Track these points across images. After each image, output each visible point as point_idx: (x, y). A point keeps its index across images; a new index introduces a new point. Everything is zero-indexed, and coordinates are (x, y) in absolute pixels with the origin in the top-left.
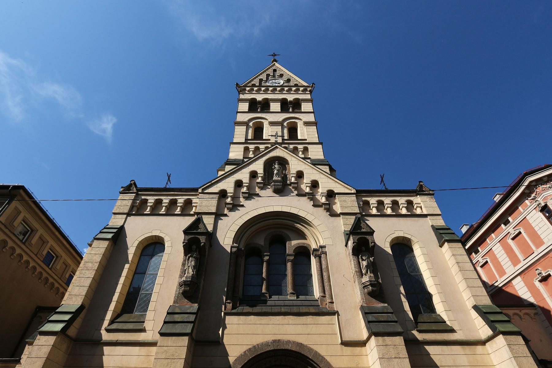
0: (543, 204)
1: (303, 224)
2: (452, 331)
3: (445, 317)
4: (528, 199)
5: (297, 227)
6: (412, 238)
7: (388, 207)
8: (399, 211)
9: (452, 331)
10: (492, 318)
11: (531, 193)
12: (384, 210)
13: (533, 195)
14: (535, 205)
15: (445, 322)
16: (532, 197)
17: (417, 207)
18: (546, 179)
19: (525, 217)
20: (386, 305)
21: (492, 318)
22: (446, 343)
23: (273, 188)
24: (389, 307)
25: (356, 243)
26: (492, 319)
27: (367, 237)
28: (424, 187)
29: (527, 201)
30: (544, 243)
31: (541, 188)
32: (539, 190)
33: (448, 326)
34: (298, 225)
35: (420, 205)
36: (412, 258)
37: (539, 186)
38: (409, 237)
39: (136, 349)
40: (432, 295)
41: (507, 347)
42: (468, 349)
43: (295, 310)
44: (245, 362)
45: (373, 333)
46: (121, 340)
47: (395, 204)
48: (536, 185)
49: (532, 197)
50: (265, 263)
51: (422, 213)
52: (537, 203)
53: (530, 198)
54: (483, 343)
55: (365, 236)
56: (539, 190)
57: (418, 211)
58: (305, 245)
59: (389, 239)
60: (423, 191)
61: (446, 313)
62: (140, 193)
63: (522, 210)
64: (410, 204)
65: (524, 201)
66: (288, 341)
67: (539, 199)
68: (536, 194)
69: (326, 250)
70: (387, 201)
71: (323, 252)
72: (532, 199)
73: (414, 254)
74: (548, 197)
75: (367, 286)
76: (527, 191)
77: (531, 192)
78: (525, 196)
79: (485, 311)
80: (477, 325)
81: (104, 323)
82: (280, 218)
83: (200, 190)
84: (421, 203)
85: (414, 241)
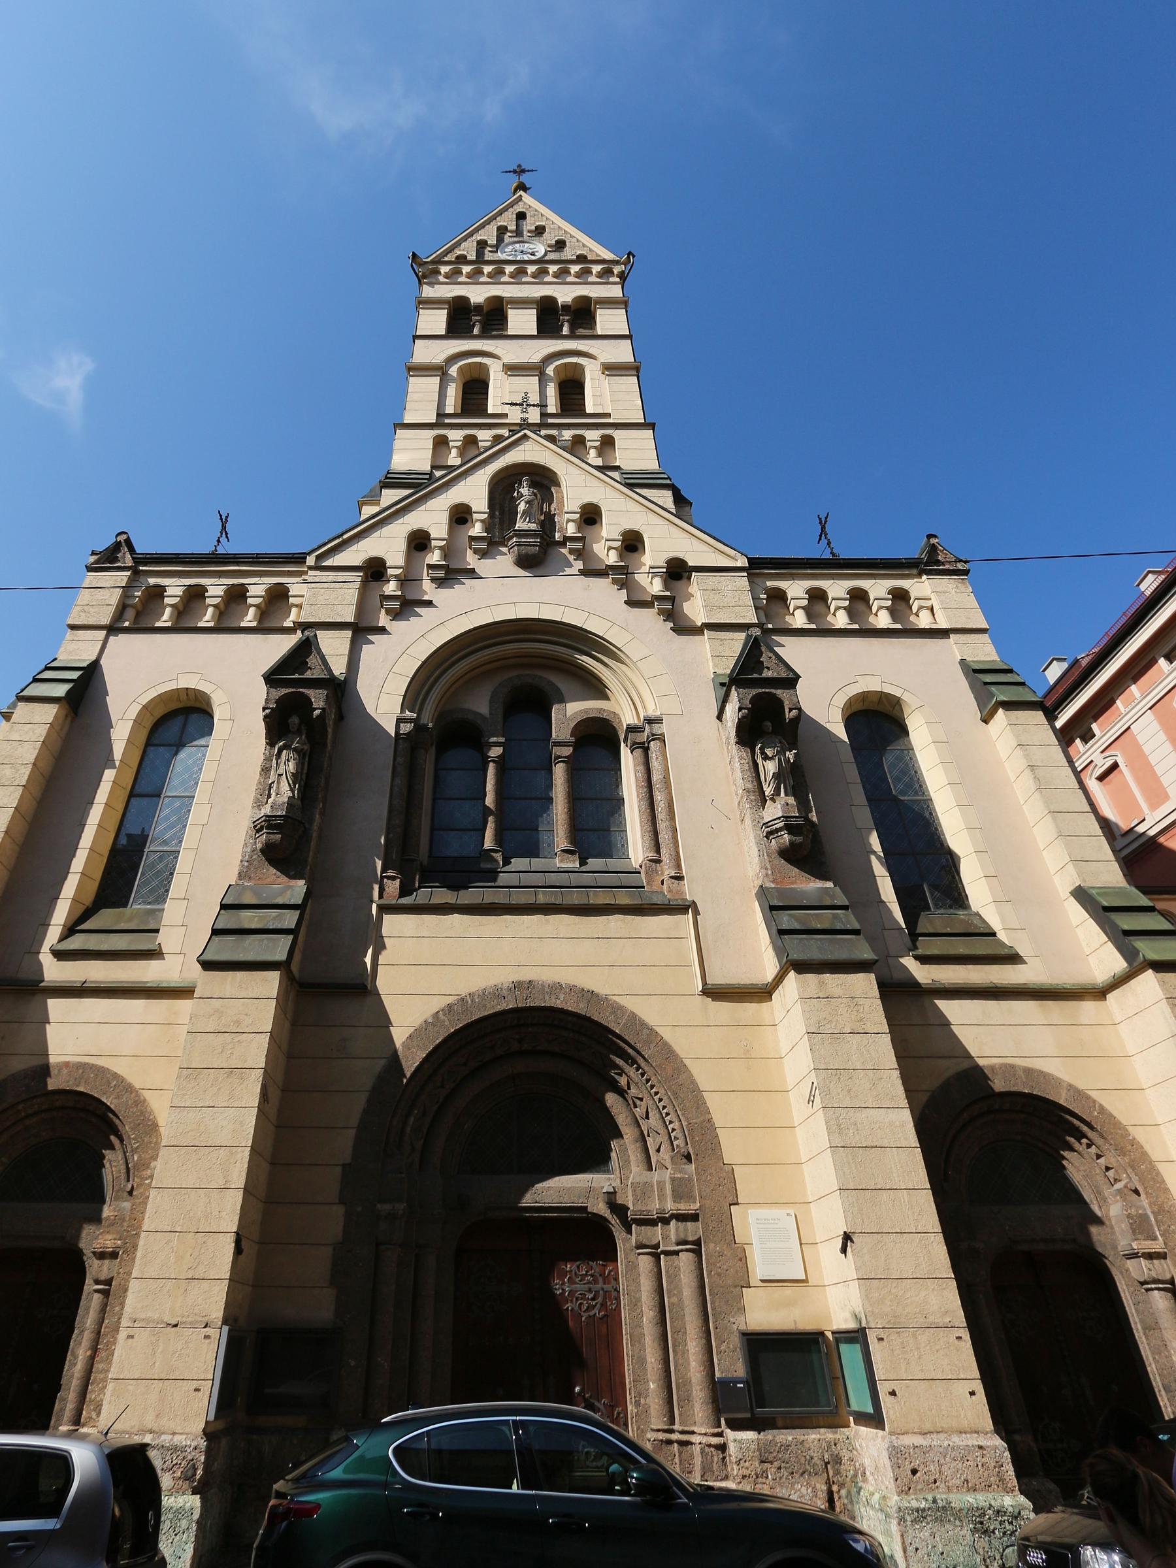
2: (1013, 958)
3: (993, 920)
6: (906, 697)
7: (838, 608)
8: (911, 619)
9: (1013, 958)
15: (994, 934)
20: (830, 885)
23: (516, 552)
25: (745, 709)
33: (1003, 944)
34: (584, 658)
35: (927, 604)
38: (897, 692)
43: (575, 898)
44: (438, 1042)
54: (1100, 993)
55: (773, 691)
57: (924, 621)
59: (841, 700)
69: (664, 728)
71: (653, 735)
73: (910, 742)
75: (777, 830)
79: (1106, 904)
83: (311, 561)
84: (933, 596)
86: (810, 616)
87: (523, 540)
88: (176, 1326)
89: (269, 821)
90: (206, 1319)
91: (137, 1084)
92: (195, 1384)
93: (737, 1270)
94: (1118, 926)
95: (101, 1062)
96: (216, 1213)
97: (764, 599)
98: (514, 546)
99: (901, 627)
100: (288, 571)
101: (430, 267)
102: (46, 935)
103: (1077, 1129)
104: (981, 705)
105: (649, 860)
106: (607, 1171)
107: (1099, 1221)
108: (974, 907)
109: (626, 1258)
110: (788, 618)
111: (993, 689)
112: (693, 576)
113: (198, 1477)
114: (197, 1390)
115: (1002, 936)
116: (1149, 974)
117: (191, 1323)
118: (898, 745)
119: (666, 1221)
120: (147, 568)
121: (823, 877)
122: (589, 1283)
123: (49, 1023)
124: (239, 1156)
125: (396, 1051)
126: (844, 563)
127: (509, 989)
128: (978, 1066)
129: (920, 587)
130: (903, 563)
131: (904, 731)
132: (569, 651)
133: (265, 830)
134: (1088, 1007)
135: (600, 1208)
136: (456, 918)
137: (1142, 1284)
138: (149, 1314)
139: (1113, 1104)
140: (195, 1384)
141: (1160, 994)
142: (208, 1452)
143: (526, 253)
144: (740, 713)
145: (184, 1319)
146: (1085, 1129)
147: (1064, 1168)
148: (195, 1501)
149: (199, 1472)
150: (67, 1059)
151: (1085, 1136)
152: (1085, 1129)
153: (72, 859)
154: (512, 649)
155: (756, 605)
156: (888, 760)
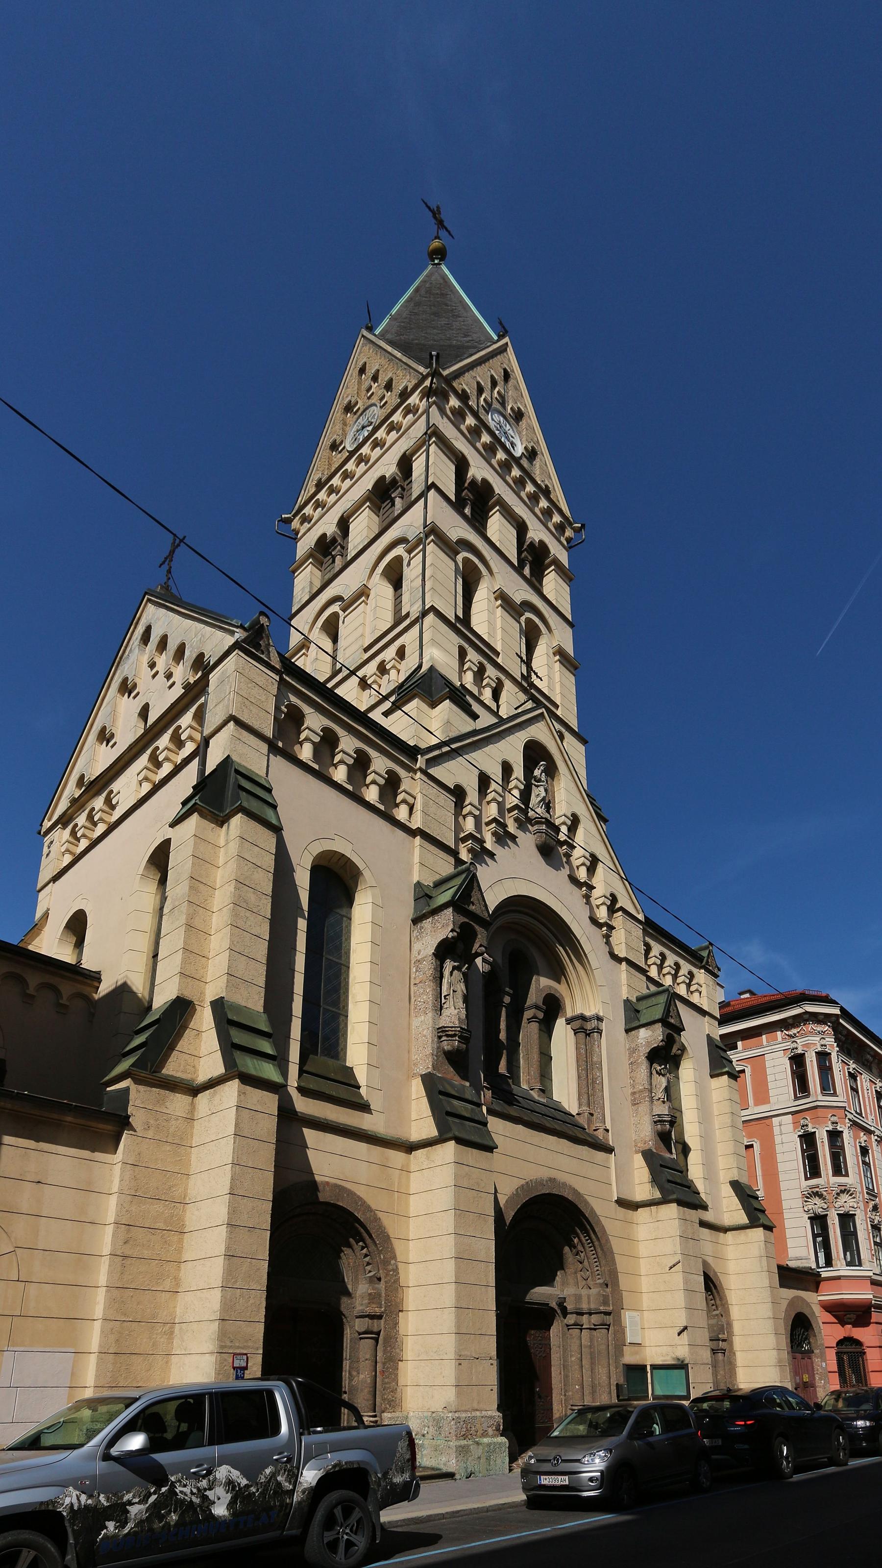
0: (800, 1051)
1: (570, 951)
2: (364, 1107)
3: (361, 1076)
4: (782, 1031)
5: (557, 952)
6: (366, 873)
7: (342, 762)
8: (330, 770)
9: (364, 1107)
10: (239, 1037)
11: (793, 1026)
12: (294, 746)
13: (794, 1031)
14: (789, 1045)
15: (699, 1194)
16: (791, 1033)
17: (404, 801)
18: (821, 1017)
19: (764, 1055)
20: (467, 1084)
21: (239, 1037)
22: (319, 1124)
23: (543, 839)
24: (264, 1017)
25: (484, 946)
26: (236, 1041)
27: (477, 927)
28: (711, 957)
29: (779, 1033)
30: (769, 1102)
31: (811, 1026)
32: (807, 1029)
33: (362, 1098)
34: (561, 948)
35: (410, 800)
36: (345, 919)
37: (809, 1024)
38: (361, 865)
39: (361, 1148)
40: (690, 1150)
41: (762, 1244)
42: (377, 1151)
43: (536, 1118)
44: (519, 1207)
45: (232, 1072)
46: (337, 1123)
47: (361, 764)
48: (807, 1020)
49: (791, 1033)
50: (504, 1009)
51: (408, 824)
52: (795, 1045)
53: (787, 1033)
54: (410, 1148)
55: (477, 927)
56: (807, 1029)
57: (401, 813)
58: (557, 995)
59: (317, 848)
60: (257, 647)
61: (704, 1182)
62: (287, 679)
63: (765, 1043)
64: (391, 784)
65: (776, 1031)
66: (563, 1184)
67: (798, 1041)
68: (798, 1032)
69: (603, 1026)
70: (348, 744)
71: (598, 1029)
72: (788, 1035)
73: (351, 914)
74: (812, 1046)
75: (665, 1121)
76: (790, 1021)
77: (794, 1024)
78: (784, 1025)
79: (748, 1193)
80: (724, 1207)
81: (290, 1070)
82: (549, 925)
83: (421, 762)
84: (704, 986)
85: (688, 1054)
86: (350, 778)
87: (549, 831)
88: (478, 1359)
89: (461, 1032)
90: (489, 1355)
91: (374, 1207)
92: (491, 1387)
93: (797, 1347)
94: (753, 1205)
95: (348, 1186)
96: (485, 1299)
97: (284, 713)
98: (542, 832)
99: (383, 809)
100: (402, 761)
101: (443, 386)
102: (288, 1070)
103: (360, 1234)
104: (628, 1020)
105: (589, 1113)
106: (553, 1286)
107: (348, 1294)
108: (349, 1061)
109: (562, 1330)
110: (331, 769)
111: (243, 794)
112: (234, 653)
113: (501, 1429)
114: (492, 1390)
115: (363, 1091)
116: (452, 1143)
117: (484, 1357)
118: (343, 912)
119: (590, 1314)
120: (290, 681)
121: (465, 1077)
122: (540, 1340)
123: (308, 1148)
124: (491, 1267)
125: (501, 1209)
126: (699, 957)
127: (547, 1181)
128: (315, 1182)
129: (701, 976)
130: (697, 956)
131: (350, 901)
132: (554, 939)
133: (457, 1039)
134: (396, 1157)
135: (554, 1305)
136: (520, 1127)
137: (360, 1334)
138: (466, 1353)
139: (389, 1224)
140: (491, 1387)
141: (763, 1239)
142: (504, 1418)
143: (507, 438)
144: (661, 1043)
145: (481, 1356)
146: (365, 1235)
147: (340, 1258)
148: (503, 1440)
149: (501, 1427)
150: (327, 1179)
151: (363, 1240)
152: (365, 1235)
153: (292, 1003)
154: (525, 920)
155: (277, 716)
156: (331, 919)
